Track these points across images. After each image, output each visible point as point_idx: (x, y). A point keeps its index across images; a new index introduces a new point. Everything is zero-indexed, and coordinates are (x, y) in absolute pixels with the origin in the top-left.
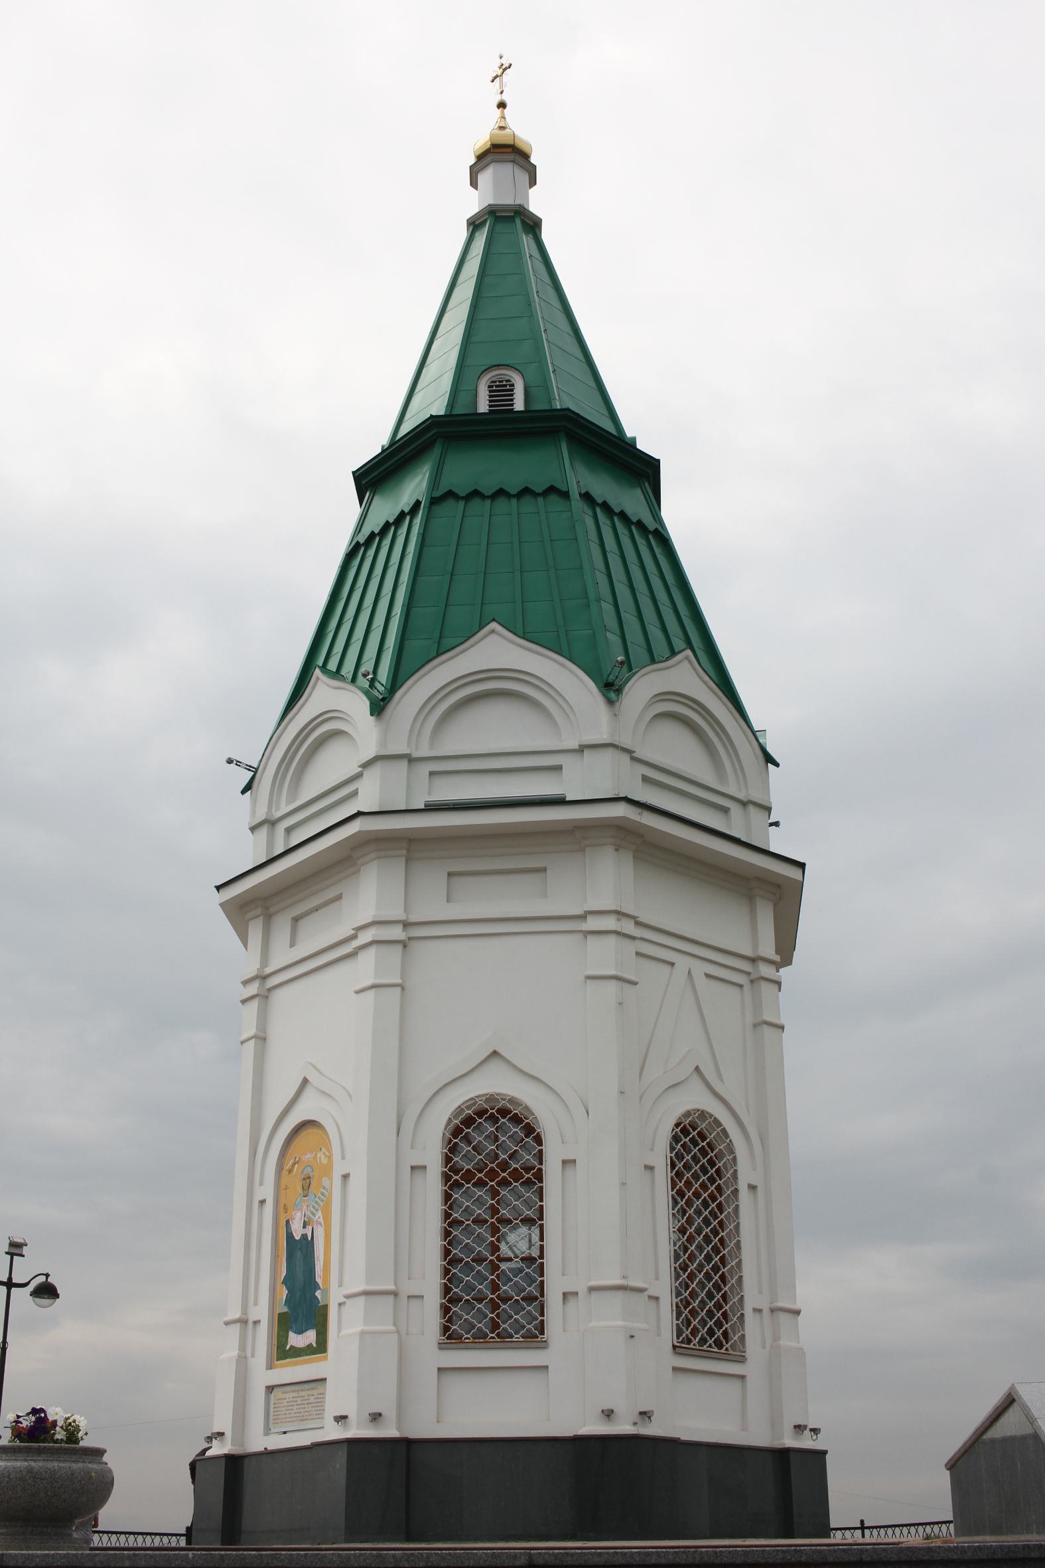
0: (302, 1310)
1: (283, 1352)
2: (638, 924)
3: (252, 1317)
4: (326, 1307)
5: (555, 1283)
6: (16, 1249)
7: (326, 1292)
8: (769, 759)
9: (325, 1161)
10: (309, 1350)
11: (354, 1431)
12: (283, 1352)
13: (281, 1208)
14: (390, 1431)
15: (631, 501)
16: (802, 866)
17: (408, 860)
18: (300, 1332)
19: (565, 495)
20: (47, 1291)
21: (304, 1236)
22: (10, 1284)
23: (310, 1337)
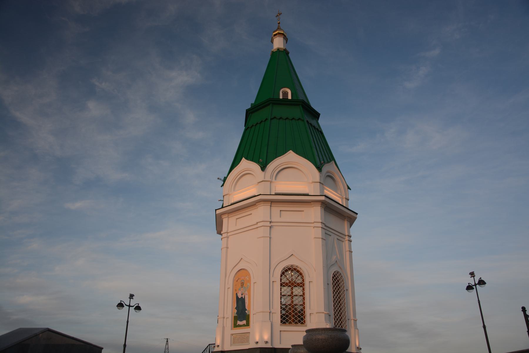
0: (241, 314)
1: (236, 326)
2: (325, 226)
3: (226, 316)
4: (249, 315)
5: (308, 311)
6: (131, 296)
7: (249, 311)
8: (349, 188)
9: (248, 279)
10: (244, 325)
11: (259, 346)
12: (236, 326)
13: (235, 290)
14: (269, 346)
15: (313, 122)
16: (357, 214)
17: (271, 206)
18: (241, 321)
19: (303, 121)
20: (138, 308)
21: (242, 297)
22: (129, 306)
23: (244, 322)
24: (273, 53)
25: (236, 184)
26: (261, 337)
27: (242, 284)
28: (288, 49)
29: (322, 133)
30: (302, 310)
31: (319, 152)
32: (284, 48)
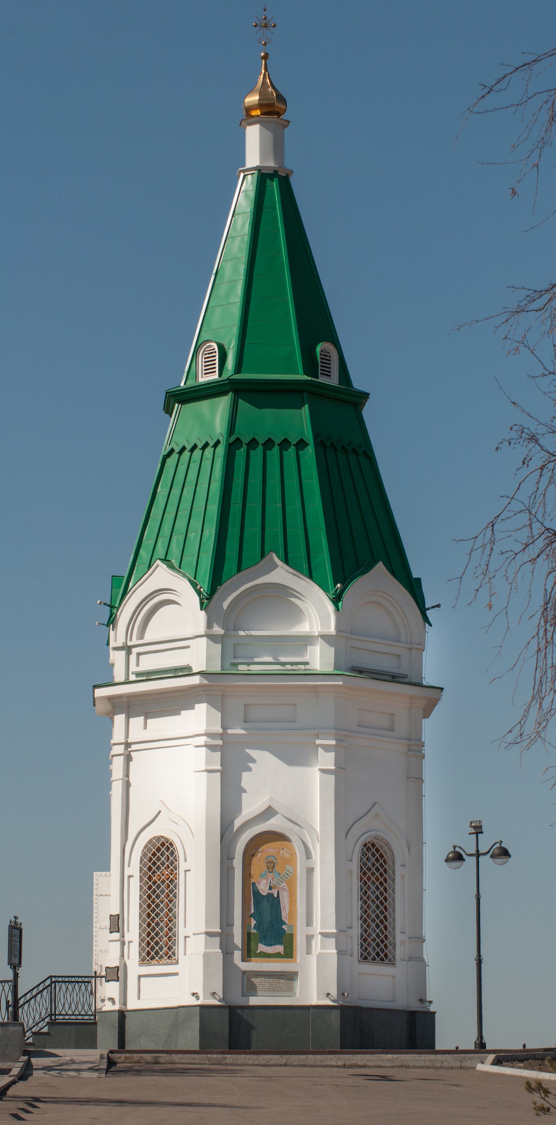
21: (270, 895)
23: (279, 948)
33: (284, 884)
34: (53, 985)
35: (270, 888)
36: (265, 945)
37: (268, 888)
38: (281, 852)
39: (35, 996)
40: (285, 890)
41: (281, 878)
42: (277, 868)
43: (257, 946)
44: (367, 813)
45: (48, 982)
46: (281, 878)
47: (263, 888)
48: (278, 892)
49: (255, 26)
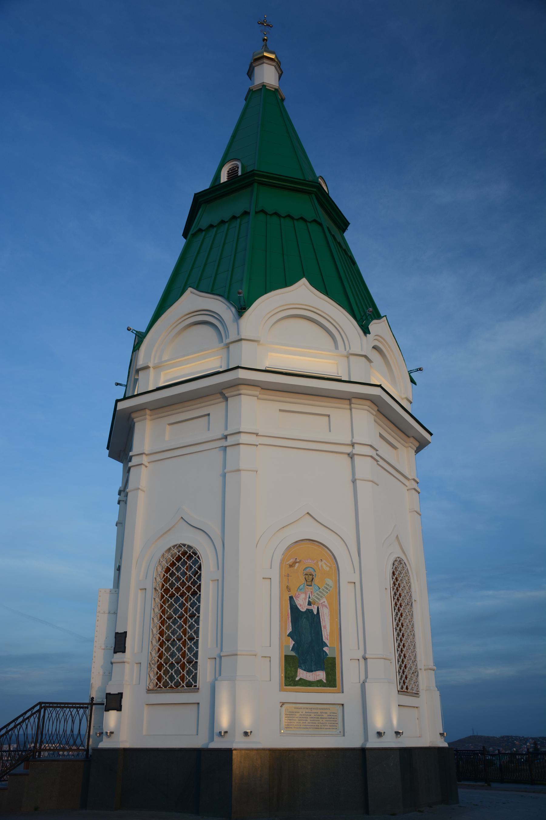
18: (310, 671)
21: (310, 611)
23: (321, 675)
24: (250, 90)
25: (174, 328)
26: (389, 720)
27: (310, 579)
28: (284, 93)
29: (354, 263)
30: (195, 573)
31: (361, 300)
32: (277, 88)
33: (324, 600)
34: (43, 710)
35: (310, 604)
36: (304, 670)
37: (307, 603)
38: (320, 563)
39: (28, 718)
40: (326, 606)
41: (320, 592)
42: (316, 581)
43: (296, 672)
44: (344, 541)
45: (38, 708)
46: (320, 592)
47: (302, 603)
48: (318, 608)
49: (264, 40)
